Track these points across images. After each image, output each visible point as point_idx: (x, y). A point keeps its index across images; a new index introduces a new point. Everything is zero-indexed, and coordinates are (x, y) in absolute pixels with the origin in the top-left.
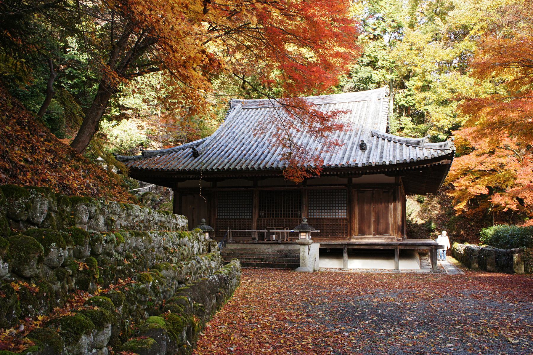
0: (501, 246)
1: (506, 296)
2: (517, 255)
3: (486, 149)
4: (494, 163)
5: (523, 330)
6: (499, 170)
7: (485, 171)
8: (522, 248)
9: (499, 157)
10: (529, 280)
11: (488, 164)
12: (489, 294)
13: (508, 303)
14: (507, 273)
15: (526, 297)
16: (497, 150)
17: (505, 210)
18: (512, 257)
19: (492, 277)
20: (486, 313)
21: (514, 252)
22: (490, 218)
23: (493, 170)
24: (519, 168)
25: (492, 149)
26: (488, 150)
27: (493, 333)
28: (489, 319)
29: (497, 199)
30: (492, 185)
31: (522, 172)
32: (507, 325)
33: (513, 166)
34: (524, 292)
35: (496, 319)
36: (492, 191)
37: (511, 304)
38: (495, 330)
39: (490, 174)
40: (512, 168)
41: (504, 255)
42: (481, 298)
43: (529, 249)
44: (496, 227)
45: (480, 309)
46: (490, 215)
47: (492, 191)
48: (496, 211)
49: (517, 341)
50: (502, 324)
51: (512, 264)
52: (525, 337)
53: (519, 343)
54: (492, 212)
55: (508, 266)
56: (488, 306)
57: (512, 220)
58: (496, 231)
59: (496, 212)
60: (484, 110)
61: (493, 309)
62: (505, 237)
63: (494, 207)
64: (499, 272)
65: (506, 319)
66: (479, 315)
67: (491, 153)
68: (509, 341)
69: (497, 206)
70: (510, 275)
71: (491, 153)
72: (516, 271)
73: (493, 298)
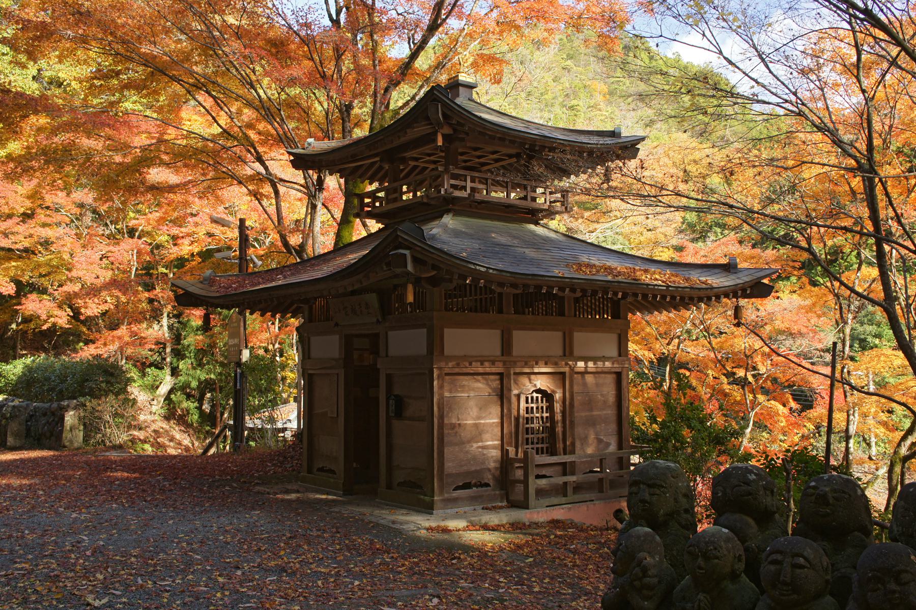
0: (36, 397)
1: (60, 498)
2: (72, 413)
3: (18, 207)
4: (31, 236)
5: (109, 570)
6: (40, 252)
7: (10, 250)
8: (82, 399)
9: (44, 225)
10: (93, 458)
11: (21, 237)
12: (23, 498)
13: (67, 512)
14: (50, 449)
15: (97, 494)
16: (39, 211)
17: (45, 327)
18: (62, 418)
19: (22, 460)
20: (26, 545)
21: (66, 409)
22: (11, 343)
23: (26, 250)
24: (78, 250)
25: (31, 209)
26: (22, 210)
27: (50, 591)
28: (36, 558)
29: (32, 305)
30: (25, 279)
31: (83, 259)
32: (75, 564)
33: (68, 244)
34: (92, 486)
35: (51, 555)
36: (23, 289)
37: (74, 515)
38: (54, 583)
39: (20, 257)
40: (66, 249)
41: (45, 415)
42: (8, 510)
43: (95, 402)
44: (29, 360)
45: (10, 536)
46: (11, 338)
47: (23, 289)
48: (26, 329)
49: (104, 601)
50: (65, 565)
51: (61, 432)
52: (117, 585)
53: (110, 601)
54: (17, 331)
55: (52, 435)
56: (27, 528)
57: (55, 347)
58: (29, 369)
59: (26, 332)
60: (33, 119)
61: (39, 532)
62: (48, 379)
63: (22, 322)
64: (31, 448)
65: (71, 551)
66: (11, 551)
67: (27, 216)
68: (88, 604)
69: (27, 320)
70: (56, 453)
71: (27, 216)
72: (67, 444)
73: (33, 507)
